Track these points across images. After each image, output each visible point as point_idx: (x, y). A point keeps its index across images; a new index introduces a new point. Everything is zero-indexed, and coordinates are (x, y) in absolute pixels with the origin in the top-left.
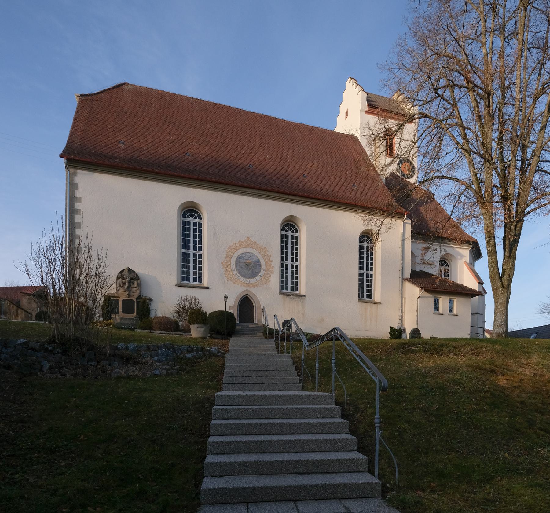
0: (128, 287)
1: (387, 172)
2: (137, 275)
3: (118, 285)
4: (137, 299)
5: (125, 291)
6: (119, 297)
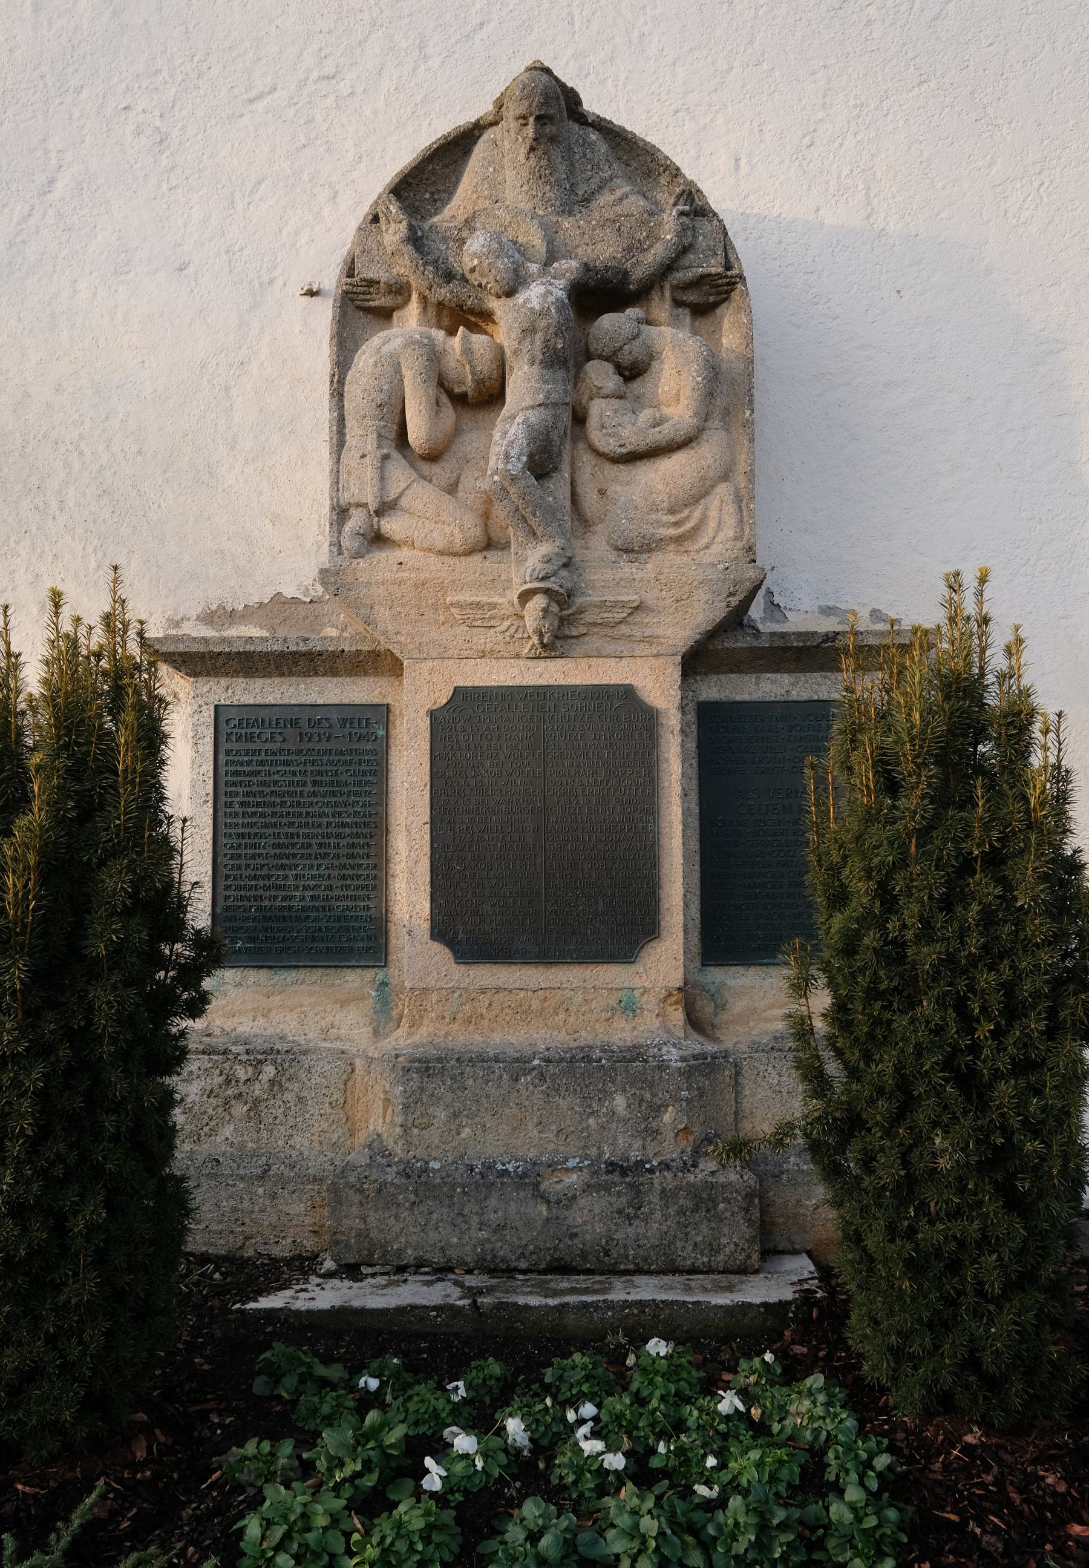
0: (542, 463)
1: (495, 462)
2: (694, 207)
3: (363, 436)
4: (697, 661)
6: (379, 662)
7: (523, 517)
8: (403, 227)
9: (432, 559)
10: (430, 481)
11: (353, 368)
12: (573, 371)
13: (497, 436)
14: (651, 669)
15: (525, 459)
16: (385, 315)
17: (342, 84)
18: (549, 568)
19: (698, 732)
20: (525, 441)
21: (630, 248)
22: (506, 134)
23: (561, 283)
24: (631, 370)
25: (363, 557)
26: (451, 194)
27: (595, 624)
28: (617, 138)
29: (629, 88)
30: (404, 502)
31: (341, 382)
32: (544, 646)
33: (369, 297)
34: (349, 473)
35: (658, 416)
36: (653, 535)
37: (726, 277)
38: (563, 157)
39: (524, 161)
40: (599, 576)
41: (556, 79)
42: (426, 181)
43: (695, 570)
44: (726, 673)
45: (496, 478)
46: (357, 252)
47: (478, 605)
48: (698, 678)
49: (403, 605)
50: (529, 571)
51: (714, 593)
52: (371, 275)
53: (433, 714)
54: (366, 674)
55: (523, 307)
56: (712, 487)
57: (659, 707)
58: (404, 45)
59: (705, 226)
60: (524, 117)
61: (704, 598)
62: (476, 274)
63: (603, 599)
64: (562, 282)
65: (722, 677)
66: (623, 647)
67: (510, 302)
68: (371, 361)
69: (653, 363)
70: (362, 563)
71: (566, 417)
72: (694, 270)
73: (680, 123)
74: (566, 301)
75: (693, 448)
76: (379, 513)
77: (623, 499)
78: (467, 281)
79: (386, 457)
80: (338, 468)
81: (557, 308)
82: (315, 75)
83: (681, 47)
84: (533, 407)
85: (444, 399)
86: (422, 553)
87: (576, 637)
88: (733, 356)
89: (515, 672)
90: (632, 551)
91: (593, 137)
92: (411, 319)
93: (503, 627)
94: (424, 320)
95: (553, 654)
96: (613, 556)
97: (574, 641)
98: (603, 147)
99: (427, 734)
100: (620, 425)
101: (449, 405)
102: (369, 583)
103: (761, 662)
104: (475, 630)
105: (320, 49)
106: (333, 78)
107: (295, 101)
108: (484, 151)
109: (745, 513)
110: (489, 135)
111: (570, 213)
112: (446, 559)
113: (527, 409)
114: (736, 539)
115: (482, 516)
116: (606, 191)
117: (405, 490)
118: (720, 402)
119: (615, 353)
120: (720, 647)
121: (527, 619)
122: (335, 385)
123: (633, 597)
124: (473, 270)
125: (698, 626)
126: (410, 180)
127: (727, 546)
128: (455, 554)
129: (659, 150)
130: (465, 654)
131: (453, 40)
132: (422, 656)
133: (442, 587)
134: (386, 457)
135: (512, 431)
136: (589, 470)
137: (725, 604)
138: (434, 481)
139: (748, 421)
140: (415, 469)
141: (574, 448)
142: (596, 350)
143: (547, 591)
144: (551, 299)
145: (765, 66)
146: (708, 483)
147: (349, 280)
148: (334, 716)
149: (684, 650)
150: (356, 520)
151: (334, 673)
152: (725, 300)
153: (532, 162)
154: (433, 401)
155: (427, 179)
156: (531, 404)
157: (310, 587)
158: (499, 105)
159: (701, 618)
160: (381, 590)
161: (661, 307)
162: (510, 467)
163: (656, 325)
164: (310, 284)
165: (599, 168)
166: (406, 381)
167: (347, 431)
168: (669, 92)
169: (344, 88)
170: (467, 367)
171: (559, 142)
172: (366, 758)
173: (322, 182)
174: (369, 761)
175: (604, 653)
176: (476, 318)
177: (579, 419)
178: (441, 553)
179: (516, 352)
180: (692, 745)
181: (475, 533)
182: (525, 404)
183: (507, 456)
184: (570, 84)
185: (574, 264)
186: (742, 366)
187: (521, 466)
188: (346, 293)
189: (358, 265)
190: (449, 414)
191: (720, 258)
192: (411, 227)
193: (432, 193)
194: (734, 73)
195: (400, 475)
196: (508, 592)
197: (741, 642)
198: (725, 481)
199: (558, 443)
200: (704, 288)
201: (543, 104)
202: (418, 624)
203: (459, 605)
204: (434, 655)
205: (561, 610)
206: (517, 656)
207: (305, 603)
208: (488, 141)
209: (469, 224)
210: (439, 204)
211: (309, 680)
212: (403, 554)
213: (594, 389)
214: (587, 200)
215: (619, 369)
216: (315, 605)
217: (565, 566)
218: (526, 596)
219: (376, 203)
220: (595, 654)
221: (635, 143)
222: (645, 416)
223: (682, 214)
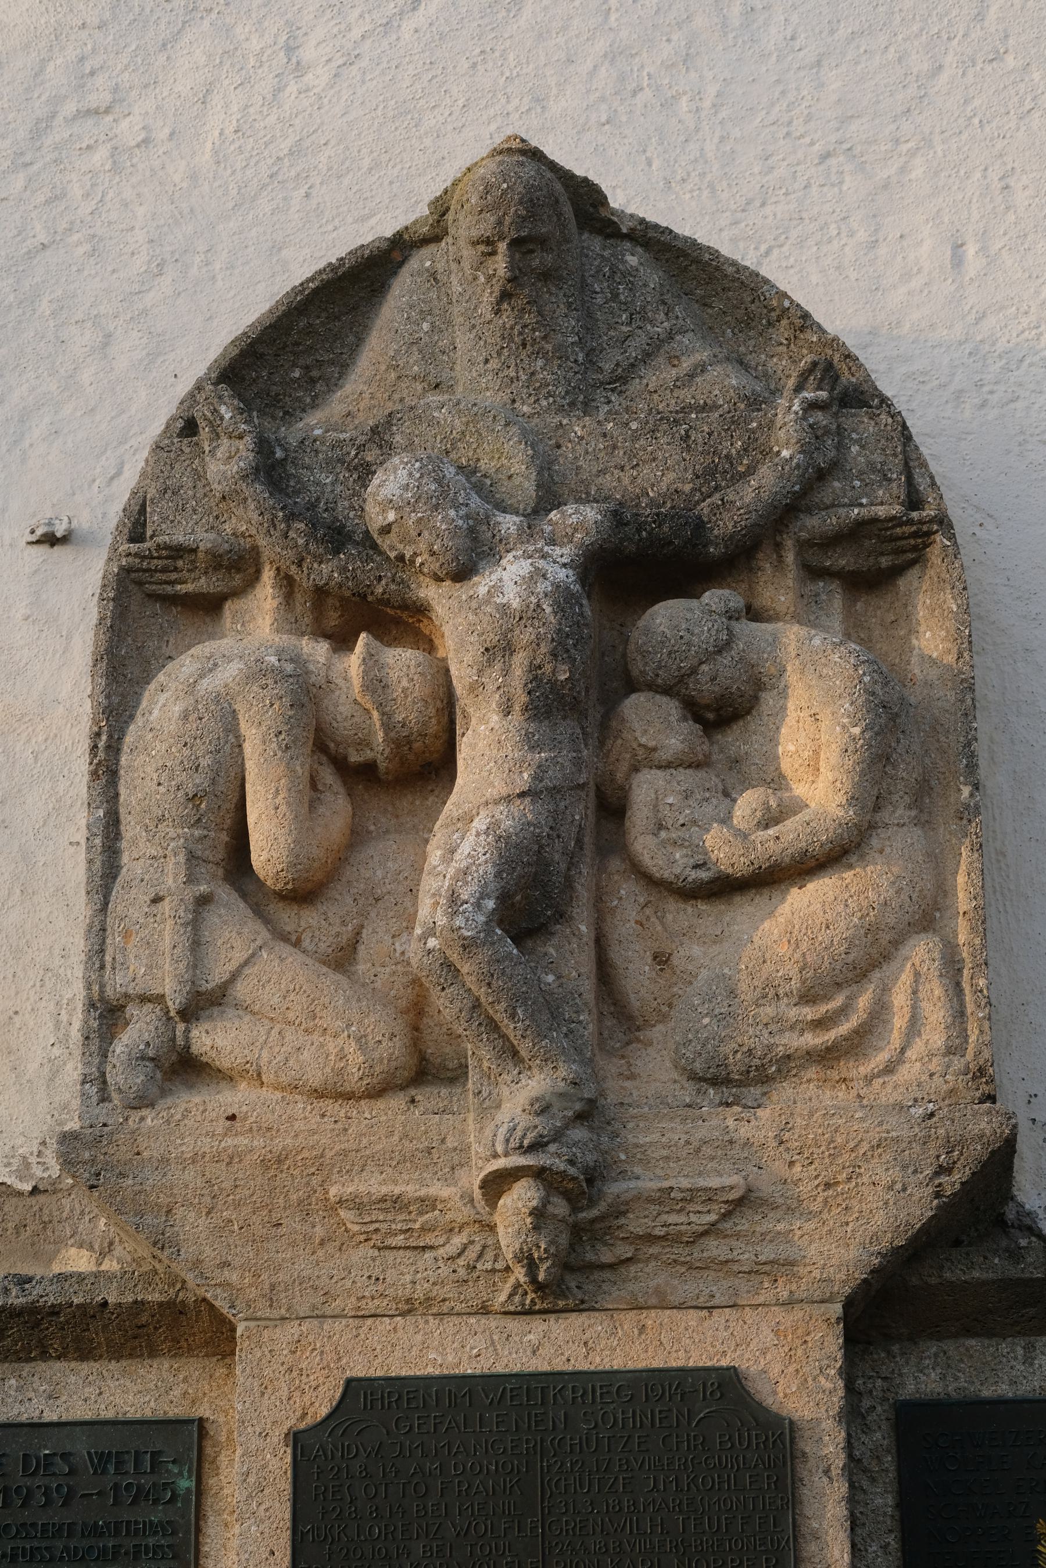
0: (528, 903)
1: (429, 910)
2: (844, 391)
3: (156, 859)
4: (880, 1313)
5: (424, 1070)
6: (183, 1325)
7: (492, 1019)
8: (245, 447)
9: (300, 1106)
10: (297, 944)
11: (139, 720)
12: (595, 714)
13: (435, 855)
14: (776, 1333)
15: (490, 904)
16: (208, 607)
17: (124, 124)
18: (543, 1126)
19: (899, 1470)
20: (490, 869)
21: (710, 472)
22: (454, 266)
23: (564, 553)
24: (717, 710)
25: (152, 1105)
26: (344, 367)
27: (650, 1239)
28: (684, 263)
29: (723, 114)
30: (241, 990)
31: (114, 748)
32: (539, 1287)
33: (174, 576)
34: (127, 934)
35: (773, 803)
36: (770, 1047)
37: (910, 522)
38: (569, 305)
39: (489, 316)
40: (655, 1137)
41: (553, 166)
42: (294, 347)
43: (862, 1120)
44: (956, 1336)
45: (432, 943)
46: (152, 493)
47: (397, 1203)
48: (895, 1348)
49: (237, 1205)
50: (502, 1131)
51: (905, 1167)
52: (179, 537)
53: (297, 1439)
54: (153, 1353)
55: (487, 602)
56: (896, 943)
57: (795, 1416)
58: (255, 44)
59: (864, 425)
60: (488, 242)
61: (885, 1179)
62: (393, 538)
63: (666, 1184)
64: (566, 550)
65: (949, 1345)
66: (719, 1288)
67: (462, 591)
68: (177, 709)
69: (763, 695)
70: (151, 1119)
71: (580, 811)
72: (842, 511)
73: (834, 178)
74: (576, 588)
75: (851, 867)
76: (190, 1013)
77: (704, 973)
78: (375, 546)
79: (203, 901)
80: (103, 922)
81: (556, 604)
82: (70, 108)
83: (832, 32)
84: (508, 799)
85: (328, 776)
86: (278, 1095)
87: (611, 1266)
88: (933, 674)
89: (478, 1343)
90: (727, 1081)
91: (632, 260)
92: (259, 621)
93: (451, 1249)
94: (288, 617)
95: (561, 1303)
96: (687, 1093)
97: (607, 1274)
98: (653, 278)
99: (286, 1485)
100: (694, 822)
101: (338, 787)
102: (164, 1161)
103: (1032, 1311)
104: (390, 1255)
105: (82, 59)
106: (107, 111)
107: (27, 158)
108: (412, 293)
109: (968, 998)
110: (421, 260)
111: (587, 407)
112: (331, 1107)
113: (496, 802)
114: (950, 1051)
115: (405, 1012)
116: (661, 360)
117: (246, 963)
118: (906, 772)
119: (682, 679)
120: (933, 1281)
121: (500, 1229)
122: (101, 755)
123: (726, 1179)
124: (386, 530)
125: (875, 1238)
126: (261, 349)
127: (932, 1067)
128: (348, 1096)
129: (766, 281)
130: (371, 1306)
131: (356, 33)
132: (276, 1314)
133: (321, 1166)
134: (203, 901)
135: (465, 848)
136: (632, 913)
137: (930, 1189)
138: (306, 943)
139: (967, 807)
140: (267, 921)
141: (602, 869)
142: (643, 673)
143: (539, 1174)
144: (542, 587)
145: (1010, 61)
146: (885, 937)
147: (134, 547)
148: (81, 1447)
149: (848, 1290)
150: (139, 1030)
151: (85, 1353)
152: (913, 563)
153: (507, 318)
154: (304, 784)
155: (297, 344)
156: (505, 791)
157: (33, 1160)
158: (441, 207)
159: (879, 1219)
160: (189, 1175)
161: (779, 588)
162: (459, 921)
163: (769, 620)
164: (49, 524)
165: (644, 319)
166: (248, 748)
167: (124, 844)
168: (808, 119)
169: (129, 130)
170: (375, 715)
171: (560, 278)
172: (151, 1541)
173: (79, 316)
174: (157, 1547)
175: (675, 1299)
176: (397, 619)
177: (612, 808)
178: (319, 1094)
179: (472, 689)
180: (883, 1500)
181: (390, 1049)
182: (492, 793)
183: (454, 899)
184: (579, 172)
185: (591, 514)
186: (951, 696)
187: (481, 918)
188: (126, 571)
189: (153, 518)
190: (338, 809)
191: (898, 488)
192: (263, 446)
193: (307, 368)
194: (944, 77)
195: (233, 936)
196: (461, 1173)
197: (983, 1268)
198: (925, 929)
199: (563, 866)
200: (866, 543)
201: (524, 219)
202: (271, 1246)
203: (356, 1204)
204: (303, 1310)
205: (575, 1210)
206: (484, 1310)
207: (20, 1194)
208: (419, 273)
209: (380, 436)
210: (320, 386)
211: (27, 1368)
212: (236, 1097)
213: (641, 752)
214: (624, 380)
215: (693, 710)
216: (42, 1198)
217: (581, 1117)
218: (496, 1185)
219: (191, 395)
220: (653, 1301)
221: (717, 268)
222: (747, 804)
223: (812, 406)
